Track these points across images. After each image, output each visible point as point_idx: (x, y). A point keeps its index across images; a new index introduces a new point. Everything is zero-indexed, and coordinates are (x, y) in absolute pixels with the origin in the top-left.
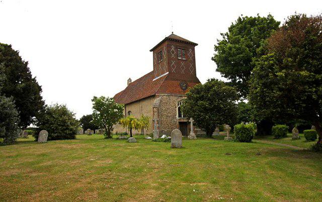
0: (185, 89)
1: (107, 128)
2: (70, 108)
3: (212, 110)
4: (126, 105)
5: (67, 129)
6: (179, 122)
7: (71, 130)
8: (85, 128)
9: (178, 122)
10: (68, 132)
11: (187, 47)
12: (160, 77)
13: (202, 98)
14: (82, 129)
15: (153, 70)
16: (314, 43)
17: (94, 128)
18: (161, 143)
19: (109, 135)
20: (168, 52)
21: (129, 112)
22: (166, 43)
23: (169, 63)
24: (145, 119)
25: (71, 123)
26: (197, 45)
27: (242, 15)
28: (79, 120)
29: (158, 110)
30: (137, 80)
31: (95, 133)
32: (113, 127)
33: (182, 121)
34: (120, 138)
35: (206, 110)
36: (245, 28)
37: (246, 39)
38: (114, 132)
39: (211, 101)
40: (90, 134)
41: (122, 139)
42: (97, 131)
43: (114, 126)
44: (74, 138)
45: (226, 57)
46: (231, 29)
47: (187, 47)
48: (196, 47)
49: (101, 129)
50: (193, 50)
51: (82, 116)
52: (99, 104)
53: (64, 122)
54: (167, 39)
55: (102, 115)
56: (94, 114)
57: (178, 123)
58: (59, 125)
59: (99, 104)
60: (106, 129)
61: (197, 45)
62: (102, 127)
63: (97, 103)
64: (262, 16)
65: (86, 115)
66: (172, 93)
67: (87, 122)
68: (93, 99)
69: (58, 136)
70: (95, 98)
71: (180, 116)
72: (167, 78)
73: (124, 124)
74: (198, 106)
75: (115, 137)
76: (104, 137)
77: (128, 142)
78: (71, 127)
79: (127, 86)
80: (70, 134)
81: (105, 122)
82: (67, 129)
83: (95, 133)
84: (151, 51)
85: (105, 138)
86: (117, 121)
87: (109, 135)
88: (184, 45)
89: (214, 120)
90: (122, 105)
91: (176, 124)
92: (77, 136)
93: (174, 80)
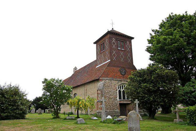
0: (124, 75)
1: (56, 108)
2: (23, 89)
3: (155, 92)
4: (74, 88)
5: (17, 109)
6: (120, 104)
7: (21, 110)
8: (37, 108)
9: (118, 104)
10: (17, 111)
11: (126, 40)
12: (102, 64)
13: (144, 81)
14: (34, 108)
15: (96, 59)
16: (137, 72)
17: (44, 108)
18: (110, 125)
19: (56, 115)
20: (110, 43)
21: (75, 94)
22: (108, 36)
23: (110, 53)
24: (91, 101)
25: (21, 103)
26: (133, 38)
27: (172, 13)
28: (32, 101)
29: (101, 93)
30: (82, 69)
31: (45, 112)
32: (61, 107)
33: (122, 102)
34: (68, 118)
35: (149, 92)
36: (176, 23)
37: (178, 31)
38: (62, 111)
39: (154, 83)
40: (40, 113)
41: (69, 119)
42: (47, 110)
43: (62, 106)
44: (23, 118)
45: (161, 46)
46: (161, 26)
47: (126, 40)
48: (132, 41)
49: (50, 109)
50: (130, 42)
51: (35, 97)
52: (49, 85)
53: (15, 102)
54: (109, 33)
55: (51, 96)
56: (44, 95)
57: (118, 105)
58: (9, 105)
59: (49, 85)
60: (54, 109)
61: (133, 38)
62: (51, 108)
63: (47, 85)
64: (189, 14)
65: (38, 97)
66: (114, 77)
67: (39, 104)
68: (43, 80)
69: (7, 116)
70: (46, 80)
71: (120, 98)
72: (109, 65)
73: (71, 105)
74: (141, 88)
75: (62, 116)
76: (52, 117)
77: (77, 123)
78: (22, 107)
79: (72, 73)
80: (20, 114)
81: (54, 103)
82: (17, 109)
83: (45, 112)
84: (95, 43)
85: (54, 118)
86: (66, 101)
87: (56, 115)
88: (124, 38)
89: (158, 102)
90: (70, 87)
91: (117, 105)
92: (27, 116)
93: (115, 66)
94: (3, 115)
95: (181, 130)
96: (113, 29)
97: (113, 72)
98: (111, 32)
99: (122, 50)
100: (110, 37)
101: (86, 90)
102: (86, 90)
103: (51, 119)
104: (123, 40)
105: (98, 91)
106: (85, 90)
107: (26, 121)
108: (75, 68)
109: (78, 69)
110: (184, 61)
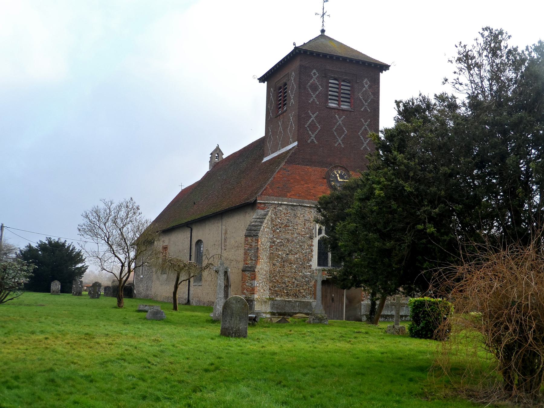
15: (260, 133)
20: (301, 86)
22: (296, 64)
26: (385, 67)
48: (384, 76)
50: (376, 83)
61: (385, 67)
79: (205, 168)
95: (415, 402)
96: (323, 31)
98: (305, 52)
99: (343, 110)
100: (301, 66)
101: (226, 233)
102: (226, 233)
106: (223, 232)
107: (82, 297)
108: (218, 151)
109: (224, 157)
110: (523, 178)
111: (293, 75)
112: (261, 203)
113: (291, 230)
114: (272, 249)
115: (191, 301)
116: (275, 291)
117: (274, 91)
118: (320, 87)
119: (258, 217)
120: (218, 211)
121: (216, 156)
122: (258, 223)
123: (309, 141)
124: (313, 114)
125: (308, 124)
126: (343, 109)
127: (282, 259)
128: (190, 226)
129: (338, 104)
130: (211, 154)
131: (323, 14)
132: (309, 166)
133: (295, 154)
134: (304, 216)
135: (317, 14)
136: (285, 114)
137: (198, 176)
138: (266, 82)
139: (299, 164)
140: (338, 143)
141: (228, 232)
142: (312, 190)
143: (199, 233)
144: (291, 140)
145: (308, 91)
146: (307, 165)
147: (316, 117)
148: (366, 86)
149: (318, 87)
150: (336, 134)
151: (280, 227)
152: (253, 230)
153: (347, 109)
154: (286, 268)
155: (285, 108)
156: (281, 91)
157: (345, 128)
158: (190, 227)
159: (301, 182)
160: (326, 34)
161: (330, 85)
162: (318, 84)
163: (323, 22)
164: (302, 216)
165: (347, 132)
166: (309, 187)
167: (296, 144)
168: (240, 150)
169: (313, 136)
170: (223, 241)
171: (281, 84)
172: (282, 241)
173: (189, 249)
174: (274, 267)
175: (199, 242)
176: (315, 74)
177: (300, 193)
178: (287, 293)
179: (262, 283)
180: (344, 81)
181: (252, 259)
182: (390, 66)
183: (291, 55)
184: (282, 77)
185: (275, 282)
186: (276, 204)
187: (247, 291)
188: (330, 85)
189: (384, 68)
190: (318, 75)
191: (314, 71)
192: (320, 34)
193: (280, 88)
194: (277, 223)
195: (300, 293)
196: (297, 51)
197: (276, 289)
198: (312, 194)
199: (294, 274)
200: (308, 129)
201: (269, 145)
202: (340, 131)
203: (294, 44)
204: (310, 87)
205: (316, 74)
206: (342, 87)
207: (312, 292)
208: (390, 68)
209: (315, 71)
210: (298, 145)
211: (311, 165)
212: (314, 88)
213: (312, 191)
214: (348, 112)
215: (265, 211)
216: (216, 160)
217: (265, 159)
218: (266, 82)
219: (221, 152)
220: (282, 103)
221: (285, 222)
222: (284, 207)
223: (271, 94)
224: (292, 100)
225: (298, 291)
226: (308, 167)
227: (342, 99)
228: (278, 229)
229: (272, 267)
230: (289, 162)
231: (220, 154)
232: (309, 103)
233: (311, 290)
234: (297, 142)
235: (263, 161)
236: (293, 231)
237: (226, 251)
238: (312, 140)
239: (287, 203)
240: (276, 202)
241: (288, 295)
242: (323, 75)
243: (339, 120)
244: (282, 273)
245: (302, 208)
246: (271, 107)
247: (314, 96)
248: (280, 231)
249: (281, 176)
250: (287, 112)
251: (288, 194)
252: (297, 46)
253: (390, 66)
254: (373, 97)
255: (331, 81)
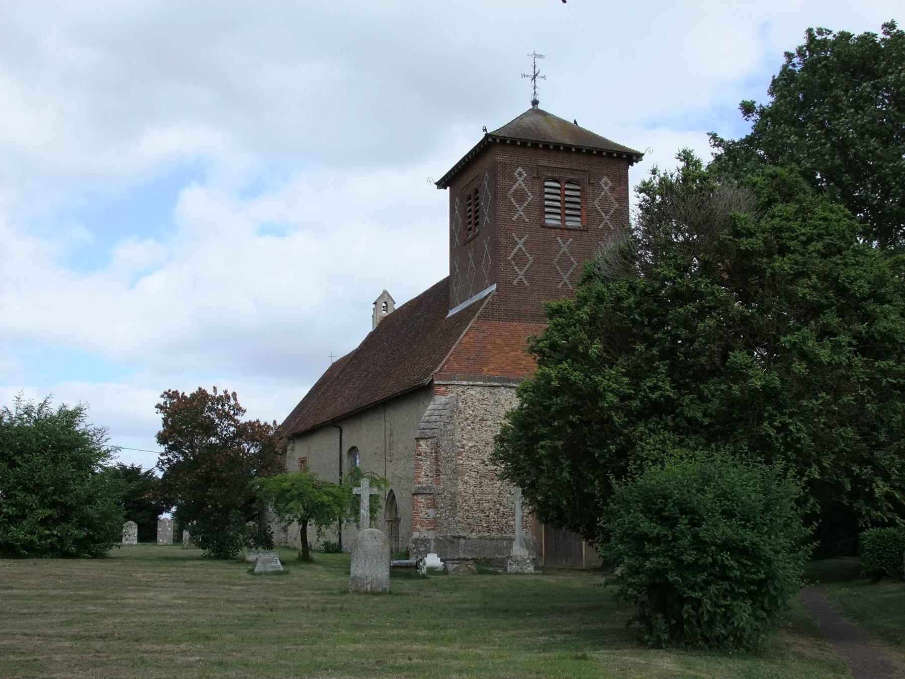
15: (442, 271)
79: (368, 328)
94: (18, 533)
96: (535, 103)
97: (507, 345)
98: (503, 141)
99: (569, 229)
102: (391, 435)
103: (198, 559)
104: (572, 171)
105: (422, 442)
106: (388, 433)
109: (397, 307)
111: (487, 178)
112: (440, 385)
113: (490, 426)
114: (460, 457)
115: (344, 546)
116: (469, 524)
117: (460, 202)
118: (529, 194)
119: (436, 407)
120: (344, 413)
121: (383, 307)
122: (436, 417)
123: (515, 282)
124: (520, 239)
125: (512, 254)
126: (570, 227)
127: (478, 472)
128: (339, 425)
129: (561, 220)
130: (375, 303)
131: (535, 76)
132: (516, 322)
133: (492, 303)
134: (511, 403)
135: (524, 76)
136: (476, 239)
137: (354, 344)
138: (448, 188)
139: (499, 319)
140: (562, 283)
141: (395, 433)
142: (523, 360)
143: (355, 435)
144: (487, 281)
145: (511, 202)
146: (513, 320)
147: (525, 244)
148: (606, 188)
149: (527, 194)
150: (559, 269)
151: (473, 423)
152: (427, 429)
153: (576, 226)
154: (484, 488)
155: (477, 230)
156: (471, 203)
157: (573, 258)
158: (339, 427)
159: (505, 348)
160: (540, 107)
161: (546, 190)
162: (526, 190)
163: (535, 88)
164: (508, 402)
165: (576, 264)
166: (517, 355)
167: (494, 287)
168: (419, 296)
169: (522, 273)
170: (388, 447)
171: (470, 191)
172: (477, 444)
173: (339, 462)
174: (465, 487)
175: (353, 450)
176: (520, 174)
177: (503, 365)
178: (487, 527)
179: (446, 512)
180: (569, 182)
181: (428, 476)
182: (643, 155)
183: (482, 147)
184: (470, 180)
185: (468, 511)
186: (464, 385)
187: (422, 526)
188: (546, 190)
189: (635, 158)
190: (526, 175)
191: (520, 169)
192: (532, 107)
193: (469, 198)
194: (468, 416)
195: (509, 526)
196: (490, 140)
197: (469, 521)
198: (522, 366)
199: (499, 497)
200: (513, 263)
201: (455, 289)
202: (565, 262)
203: (485, 130)
204: (514, 195)
205: (523, 175)
206: (566, 192)
207: (528, 525)
208: (643, 157)
209: (522, 170)
210: (497, 290)
211: (520, 321)
212: (521, 196)
213: (522, 362)
214: (579, 232)
215: (447, 397)
216: (383, 312)
217: (451, 313)
218: (448, 188)
219: (392, 299)
220: (472, 223)
221: (480, 414)
222: (478, 389)
223: (456, 208)
224: (486, 217)
225: (506, 523)
226: (515, 324)
227: (567, 212)
228: (470, 426)
229: (463, 487)
230: (484, 318)
231: (389, 302)
232: (513, 221)
233: (526, 521)
234: (495, 284)
235: (448, 316)
236: (495, 427)
237: (392, 463)
238: (521, 282)
239: (482, 383)
240: (464, 383)
241: (490, 530)
242: (535, 176)
243: (562, 246)
244: (478, 496)
245: (508, 389)
246: (457, 228)
247: (520, 209)
248: (472, 429)
249: (472, 340)
250: (479, 236)
251: (484, 368)
252: (489, 132)
253: (643, 155)
254: (618, 205)
255: (547, 184)
